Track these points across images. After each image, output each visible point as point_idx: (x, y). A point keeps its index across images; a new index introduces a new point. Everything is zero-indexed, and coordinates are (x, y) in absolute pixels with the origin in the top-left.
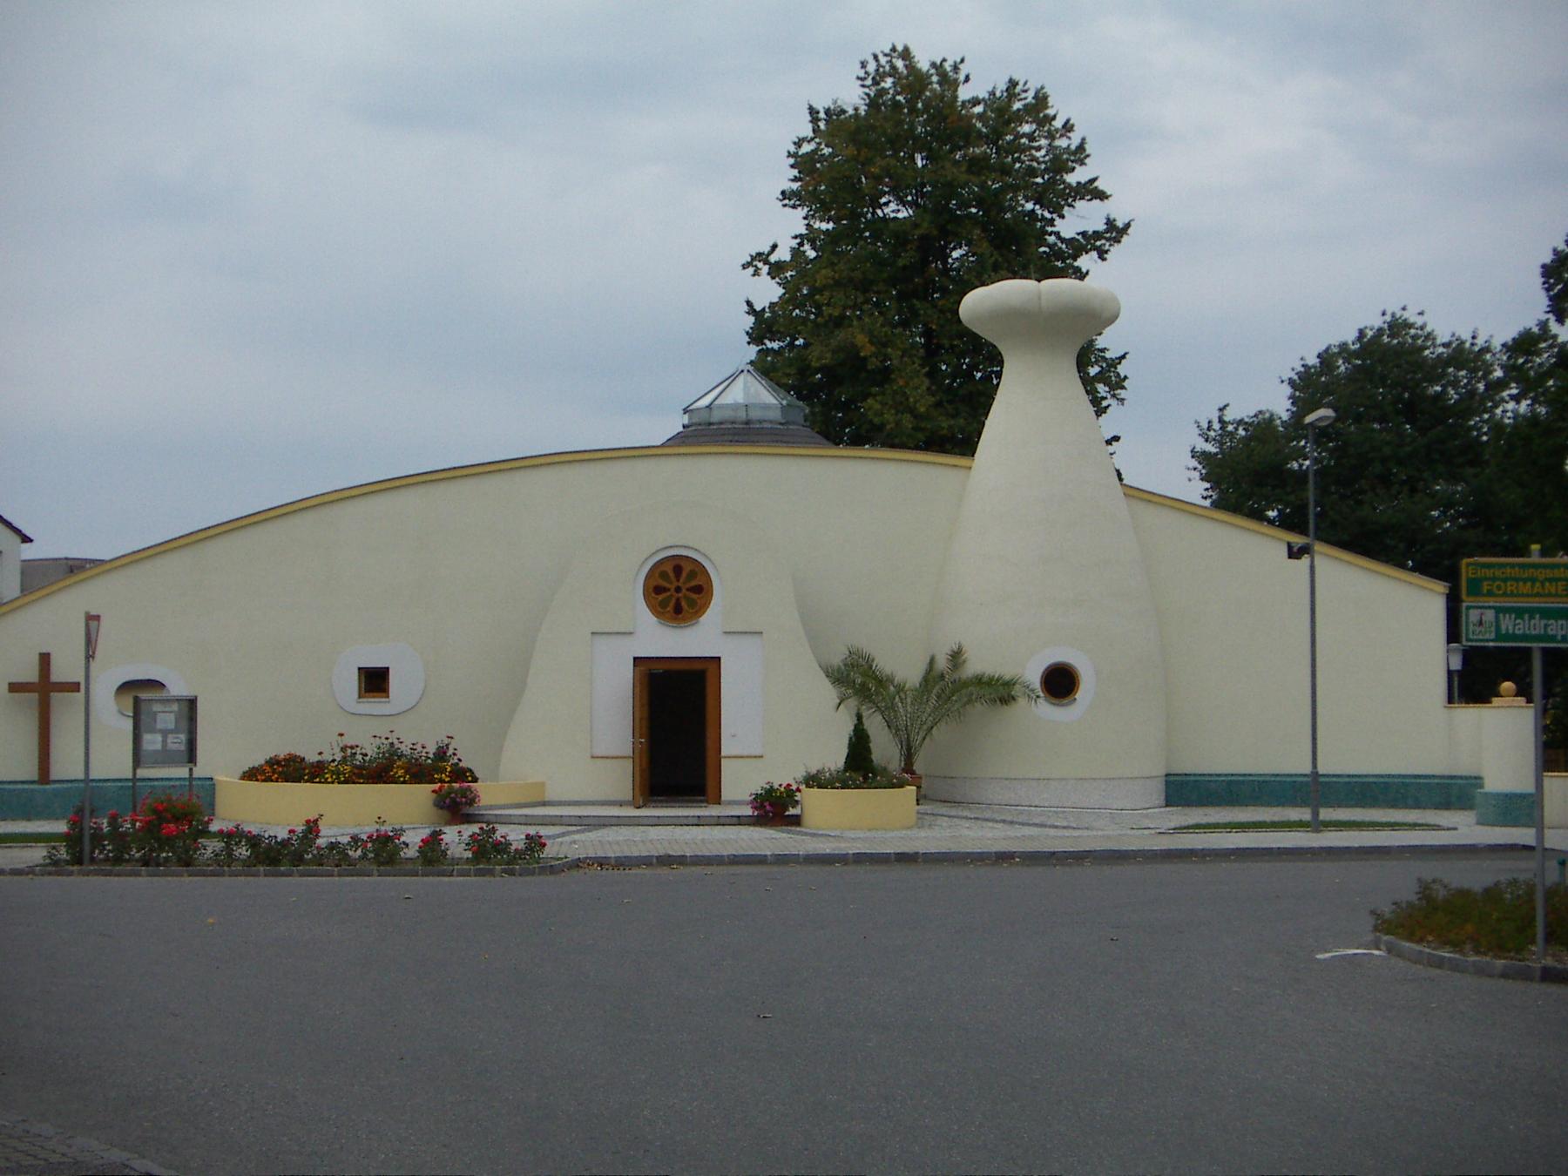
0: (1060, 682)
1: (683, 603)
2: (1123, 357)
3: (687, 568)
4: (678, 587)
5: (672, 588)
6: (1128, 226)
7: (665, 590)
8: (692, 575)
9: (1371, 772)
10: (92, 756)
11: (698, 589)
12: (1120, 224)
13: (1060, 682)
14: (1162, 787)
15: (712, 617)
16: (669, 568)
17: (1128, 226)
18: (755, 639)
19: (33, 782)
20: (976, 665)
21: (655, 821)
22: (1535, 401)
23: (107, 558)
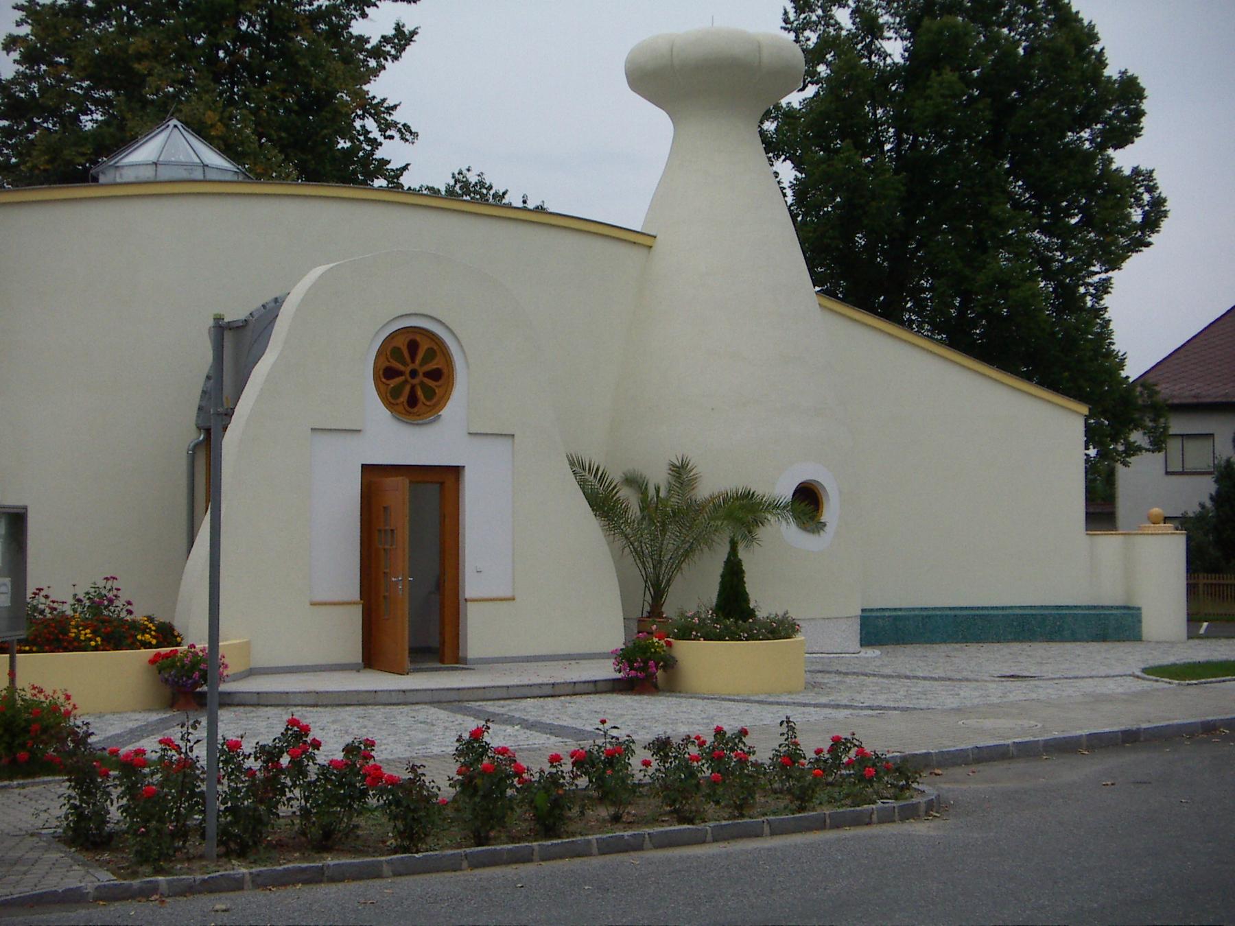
0: (808, 501)
1: (419, 393)
2: (405, 168)
3: (424, 346)
4: (414, 372)
5: (407, 370)
6: (414, 33)
7: (398, 373)
8: (431, 354)
9: (904, 605)
10: (491, 603)
11: (436, 375)
12: (406, 30)
13: (808, 501)
14: (857, 627)
15: (454, 409)
16: (402, 343)
17: (414, 33)
18: (502, 446)
19: (1172, 644)
20: (713, 482)
21: (504, 693)
22: (1002, 224)
23: (551, 210)
